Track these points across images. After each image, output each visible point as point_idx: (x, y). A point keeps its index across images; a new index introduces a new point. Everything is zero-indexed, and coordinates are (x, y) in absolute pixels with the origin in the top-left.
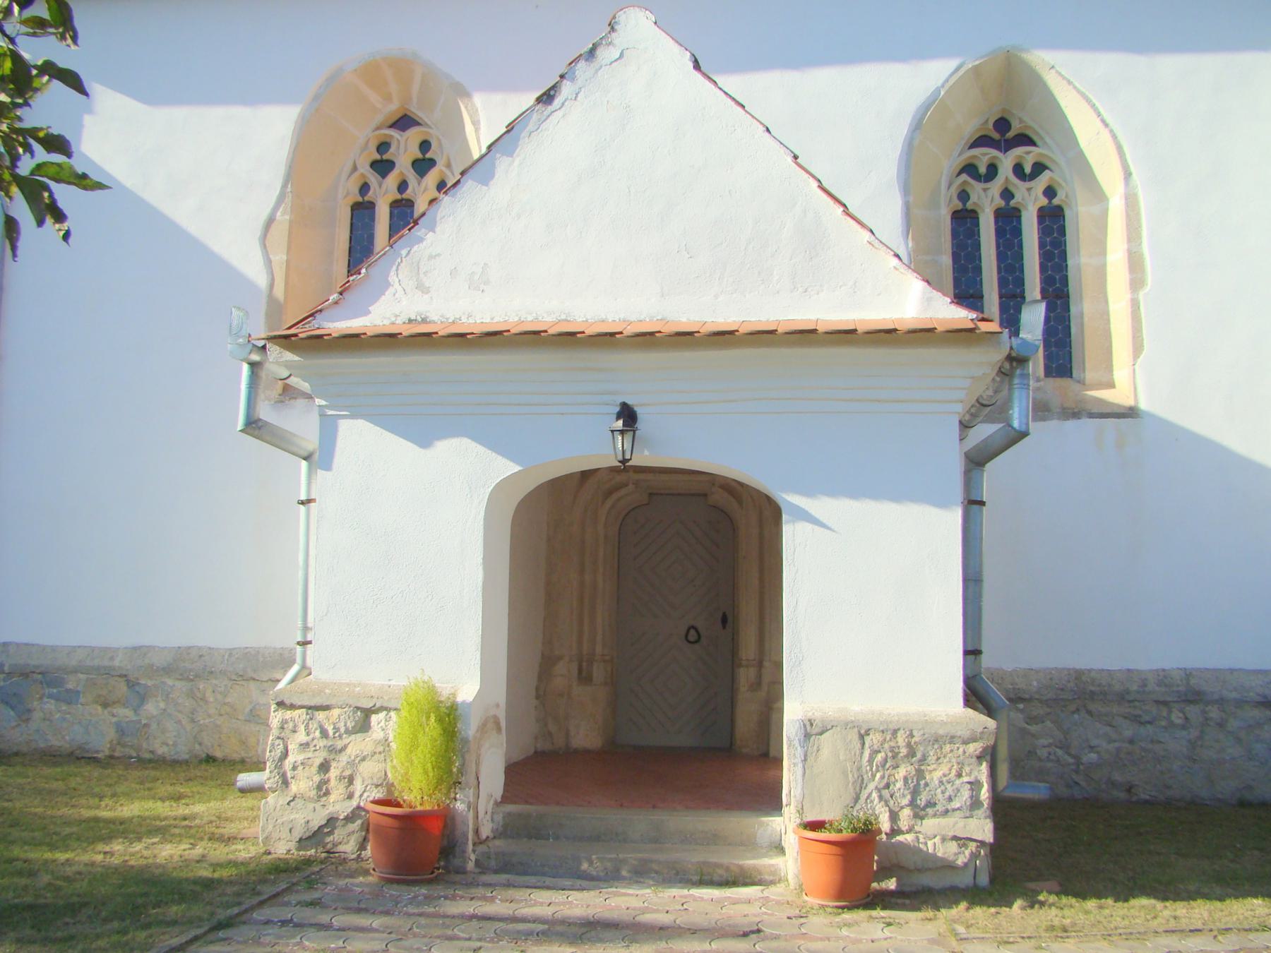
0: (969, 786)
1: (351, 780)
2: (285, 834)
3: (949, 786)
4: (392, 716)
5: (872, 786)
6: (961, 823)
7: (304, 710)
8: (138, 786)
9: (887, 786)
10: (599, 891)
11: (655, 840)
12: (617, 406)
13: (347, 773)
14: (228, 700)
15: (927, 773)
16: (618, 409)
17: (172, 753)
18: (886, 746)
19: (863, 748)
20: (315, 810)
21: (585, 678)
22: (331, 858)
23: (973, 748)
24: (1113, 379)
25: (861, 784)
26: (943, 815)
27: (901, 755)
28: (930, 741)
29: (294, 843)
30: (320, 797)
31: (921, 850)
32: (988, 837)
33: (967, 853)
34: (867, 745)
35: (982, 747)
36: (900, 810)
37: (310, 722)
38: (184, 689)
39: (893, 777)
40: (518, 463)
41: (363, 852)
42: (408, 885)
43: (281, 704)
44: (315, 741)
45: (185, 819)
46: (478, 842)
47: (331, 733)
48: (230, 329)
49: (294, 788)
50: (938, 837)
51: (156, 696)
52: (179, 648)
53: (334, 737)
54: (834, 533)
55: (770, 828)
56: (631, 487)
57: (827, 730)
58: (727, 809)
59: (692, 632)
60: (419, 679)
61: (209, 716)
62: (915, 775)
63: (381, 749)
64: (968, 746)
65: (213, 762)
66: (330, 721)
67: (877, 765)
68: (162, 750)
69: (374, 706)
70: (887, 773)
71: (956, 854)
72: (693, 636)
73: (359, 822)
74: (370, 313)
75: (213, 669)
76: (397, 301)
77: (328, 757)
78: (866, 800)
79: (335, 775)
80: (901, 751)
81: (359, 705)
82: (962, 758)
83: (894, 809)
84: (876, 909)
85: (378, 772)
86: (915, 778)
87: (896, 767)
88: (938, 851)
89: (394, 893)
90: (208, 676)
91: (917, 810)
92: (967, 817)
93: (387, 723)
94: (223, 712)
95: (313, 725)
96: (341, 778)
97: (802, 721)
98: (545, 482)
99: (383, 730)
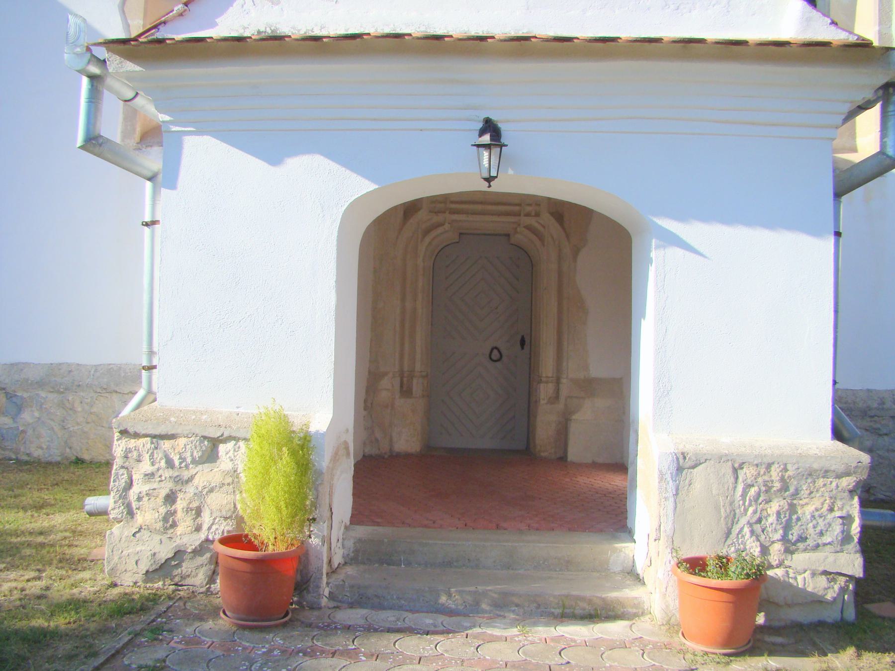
0: (840, 521)
1: (199, 512)
2: (131, 566)
3: (820, 521)
4: (241, 446)
5: (743, 521)
6: (831, 558)
7: (149, 439)
8: (6, 493)
9: (759, 521)
10: (464, 634)
11: (508, 567)
12: (479, 121)
13: (195, 505)
14: (94, 410)
15: (799, 508)
16: (480, 125)
17: (46, 456)
18: (760, 480)
19: (736, 482)
20: (161, 542)
21: (406, 391)
22: (180, 590)
23: (848, 482)
24: (856, 145)
25: (733, 518)
26: (814, 550)
27: (775, 489)
28: (803, 475)
29: (140, 575)
30: (166, 529)
31: (791, 585)
32: (859, 572)
33: (836, 587)
34: (740, 479)
35: (854, 481)
36: (770, 545)
37: (155, 451)
38: (56, 401)
39: (765, 511)
40: (374, 181)
41: (212, 586)
42: (262, 631)
43: (124, 433)
44: (161, 472)
45: (41, 533)
46: (333, 572)
47: (177, 463)
48: (67, 38)
49: (140, 519)
50: (808, 572)
51: (32, 407)
52: (52, 364)
53: (180, 468)
54: (706, 260)
55: (622, 555)
56: (447, 226)
57: (701, 464)
58: (570, 530)
59: (495, 352)
60: (270, 409)
61: (78, 424)
62: (787, 510)
63: (229, 480)
64: (841, 480)
65: (81, 464)
66: (176, 451)
67: (750, 500)
68: (37, 453)
69: (222, 435)
70: (760, 507)
71: (826, 589)
72: (496, 355)
73: (208, 555)
74: (217, 25)
75: (81, 383)
76: (245, 13)
77: (174, 488)
78: (738, 535)
79: (182, 506)
80: (775, 485)
81: (206, 434)
82: (834, 492)
83: (764, 544)
84: (763, 655)
85: (227, 504)
86: (787, 513)
87: (768, 501)
88: (808, 586)
89: (247, 644)
90: (76, 389)
91: (788, 545)
92: (838, 552)
93: (236, 454)
94: (90, 420)
95: (158, 455)
96: (188, 510)
97: (676, 455)
98: (401, 205)
99: (232, 460)
